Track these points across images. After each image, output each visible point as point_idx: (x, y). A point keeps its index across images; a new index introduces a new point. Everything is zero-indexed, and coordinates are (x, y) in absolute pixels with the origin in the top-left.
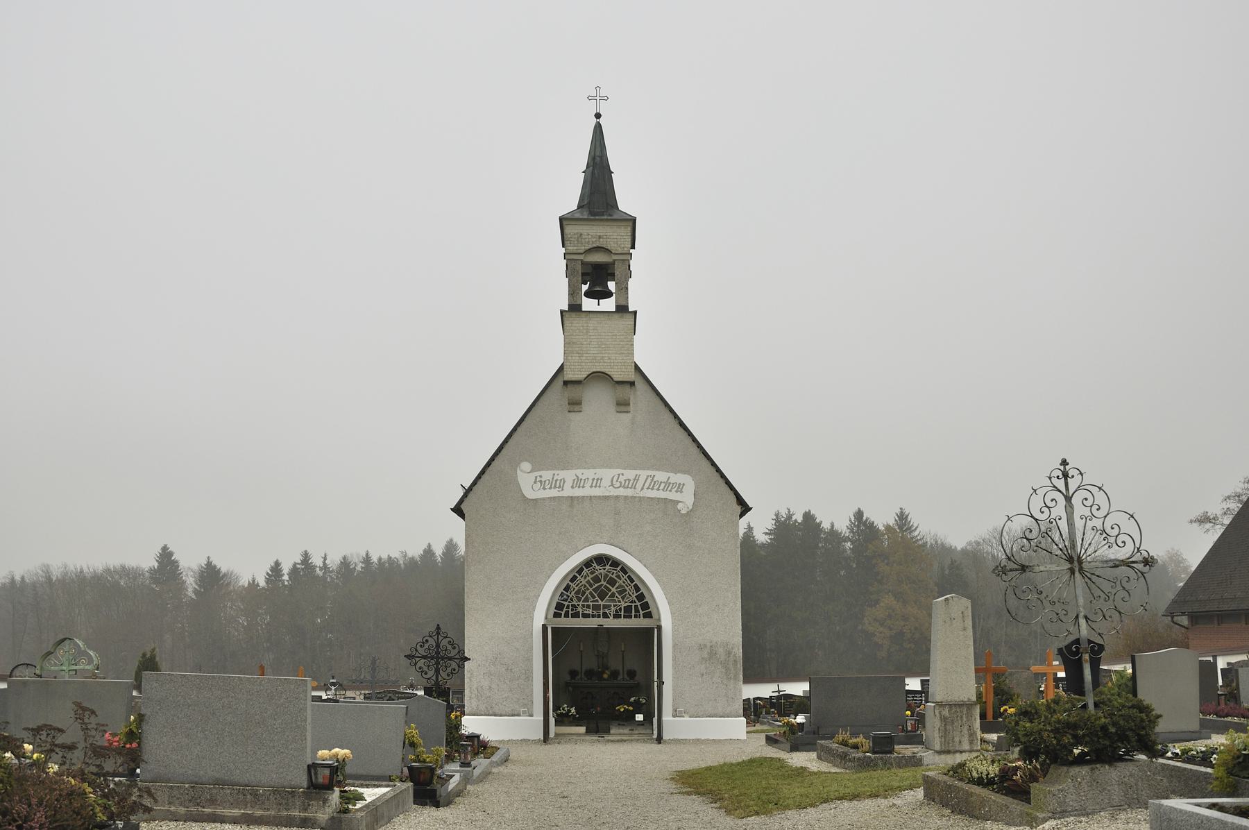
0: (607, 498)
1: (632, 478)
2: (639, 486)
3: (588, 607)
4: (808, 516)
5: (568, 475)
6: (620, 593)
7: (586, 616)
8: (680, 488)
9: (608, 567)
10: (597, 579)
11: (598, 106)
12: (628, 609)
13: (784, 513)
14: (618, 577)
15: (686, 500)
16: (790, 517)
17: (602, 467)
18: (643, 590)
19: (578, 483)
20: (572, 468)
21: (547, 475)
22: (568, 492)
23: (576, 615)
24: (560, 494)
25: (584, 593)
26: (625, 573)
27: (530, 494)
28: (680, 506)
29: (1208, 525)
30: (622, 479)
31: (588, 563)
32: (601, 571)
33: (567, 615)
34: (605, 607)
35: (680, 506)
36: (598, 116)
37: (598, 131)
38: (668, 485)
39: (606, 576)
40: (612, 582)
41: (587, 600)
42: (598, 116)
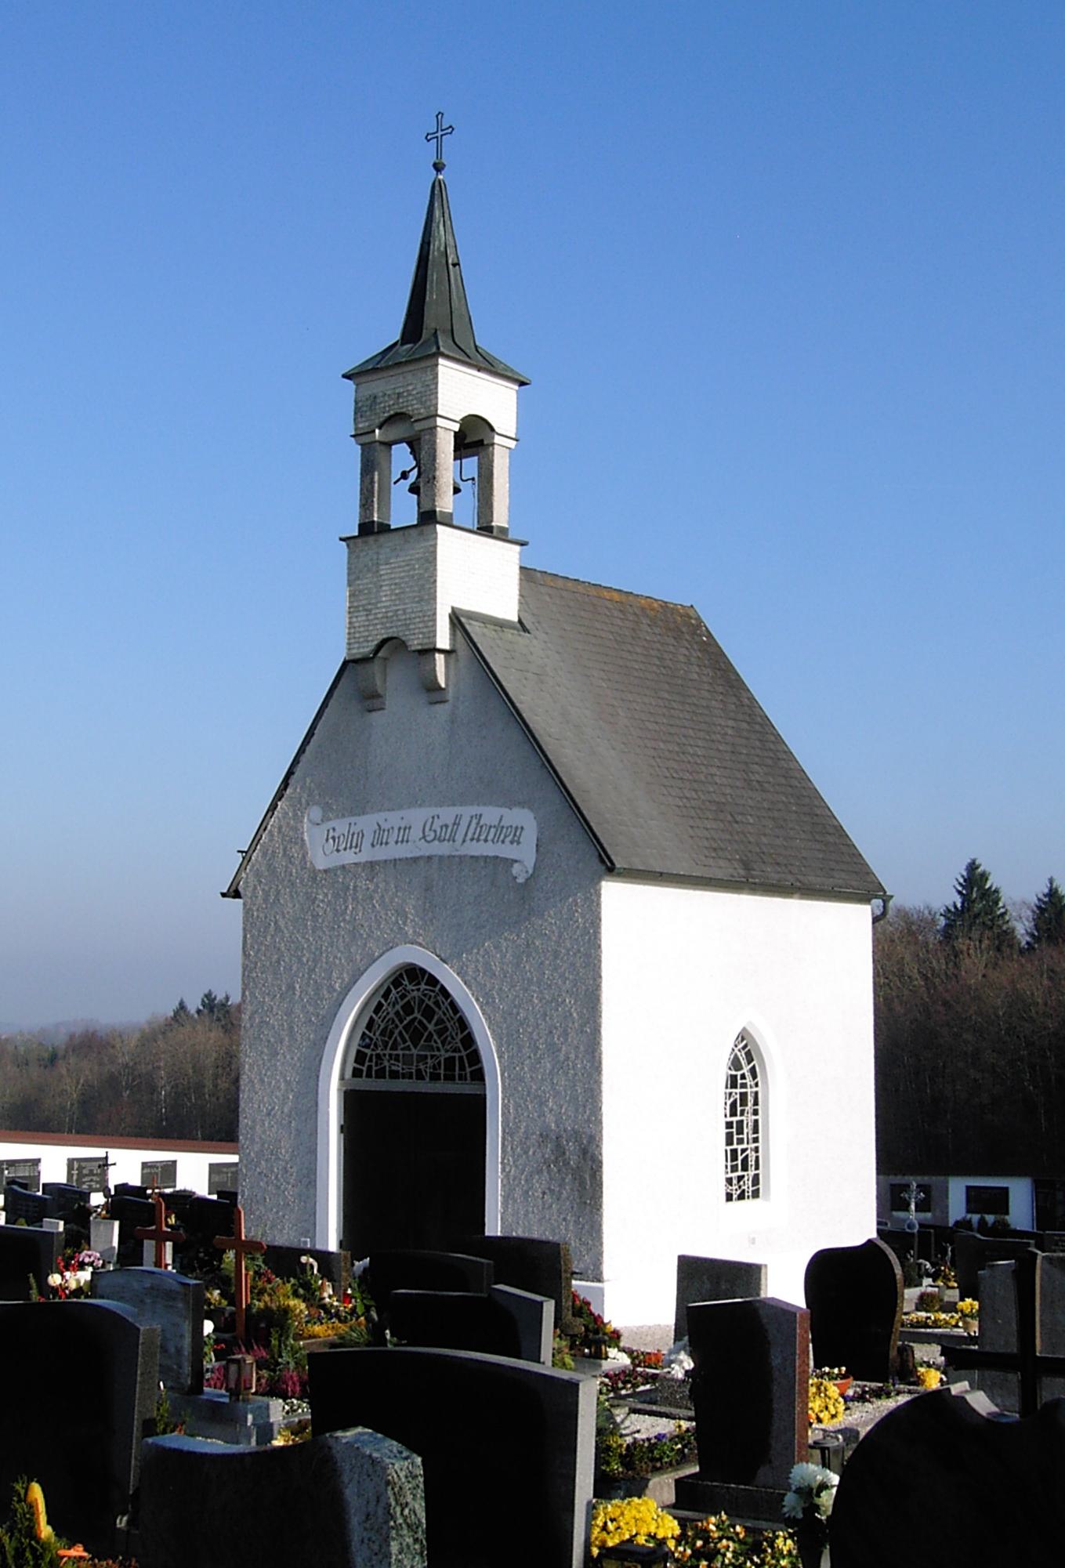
0: (415, 860)
1: (450, 822)
2: (459, 837)
5: (366, 823)
6: (440, 1033)
7: (394, 1075)
8: (516, 835)
9: (423, 986)
10: (408, 1009)
12: (450, 1062)
14: (437, 1003)
15: (524, 855)
19: (379, 841)
21: (341, 826)
23: (381, 1074)
25: (392, 1033)
32: (415, 992)
33: (369, 1075)
35: (516, 869)
37: (437, 192)
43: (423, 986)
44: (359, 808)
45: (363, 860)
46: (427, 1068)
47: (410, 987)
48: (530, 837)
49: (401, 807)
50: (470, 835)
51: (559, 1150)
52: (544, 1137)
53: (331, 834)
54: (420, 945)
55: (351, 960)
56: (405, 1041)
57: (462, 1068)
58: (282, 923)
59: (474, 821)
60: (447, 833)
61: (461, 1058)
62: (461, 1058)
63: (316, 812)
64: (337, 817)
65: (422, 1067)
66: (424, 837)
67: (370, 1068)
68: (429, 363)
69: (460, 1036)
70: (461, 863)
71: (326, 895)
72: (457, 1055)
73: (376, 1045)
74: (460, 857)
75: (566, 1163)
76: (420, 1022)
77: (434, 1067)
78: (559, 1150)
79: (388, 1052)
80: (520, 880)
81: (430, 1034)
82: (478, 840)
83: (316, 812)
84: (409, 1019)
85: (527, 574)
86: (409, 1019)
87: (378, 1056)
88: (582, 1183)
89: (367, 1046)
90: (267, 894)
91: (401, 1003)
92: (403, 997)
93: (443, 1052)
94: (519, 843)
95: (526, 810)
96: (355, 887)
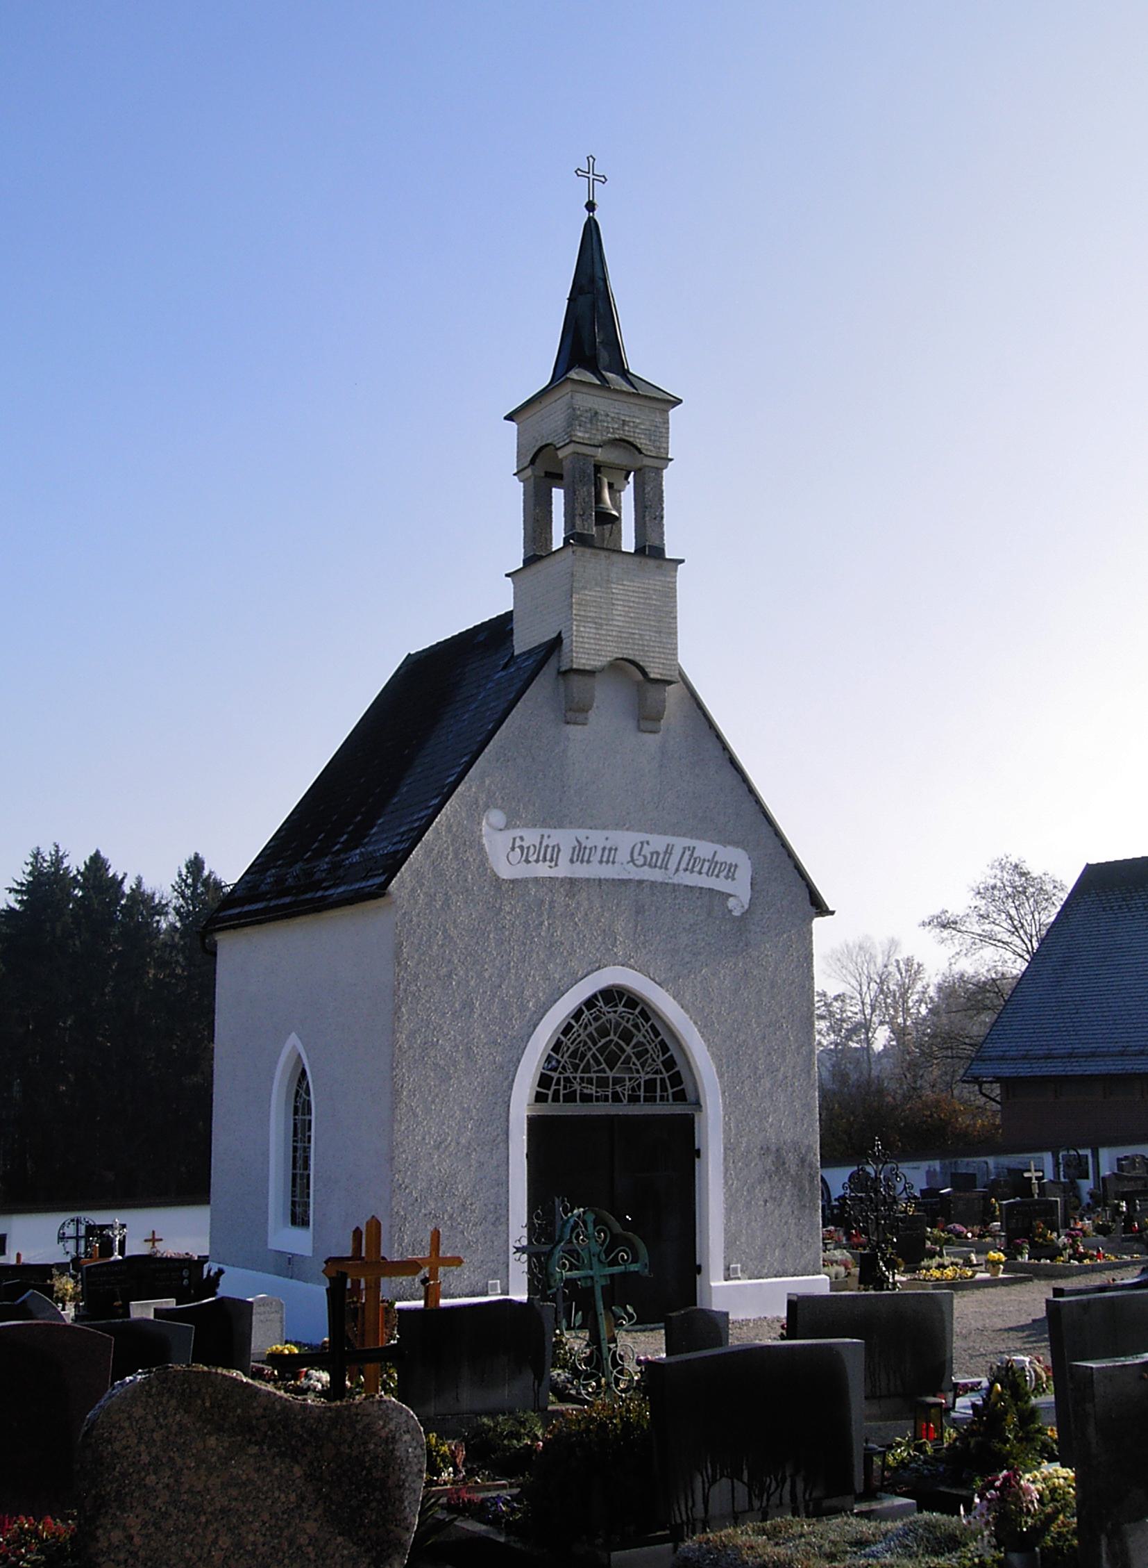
0: (624, 882)
1: (661, 850)
2: (672, 865)
3: (590, 1081)
4: (97, 863)
5: (564, 838)
6: (639, 1055)
7: (586, 1098)
8: (731, 871)
9: (620, 1009)
10: (603, 1032)
11: (591, 190)
12: (650, 1085)
13: (47, 852)
14: (636, 1026)
15: (740, 891)
16: (58, 860)
17: (619, 825)
18: (673, 1051)
19: (580, 854)
20: (573, 824)
21: (531, 837)
22: (563, 870)
23: (570, 1098)
24: (552, 873)
25: (583, 1056)
26: (647, 1019)
27: (505, 871)
28: (731, 903)
29: (946, 933)
30: (647, 850)
31: (590, 1003)
32: (610, 1014)
33: (556, 1099)
34: (617, 1081)
35: (731, 903)
36: (590, 206)
37: (591, 233)
38: (714, 866)
39: (618, 1024)
40: (627, 1036)
41: (587, 1069)
42: (590, 206)
43: (620, 1009)
44: (552, 818)
45: (561, 876)
46: (625, 1090)
47: (605, 1009)
48: (744, 874)
49: (605, 828)
50: (683, 865)
51: (780, 1161)
52: (765, 1150)
53: (518, 843)
54: (633, 968)
55: (547, 978)
56: (598, 1063)
57: (664, 1089)
58: (453, 932)
59: (688, 853)
60: (657, 860)
61: (662, 1080)
62: (662, 1080)
63: (497, 816)
64: (526, 826)
65: (619, 1090)
66: (632, 860)
67: (557, 1092)
68: (663, 406)
69: (662, 1058)
70: (674, 891)
71: (514, 907)
72: (658, 1076)
73: (564, 1067)
74: (674, 885)
75: (787, 1172)
76: (617, 1044)
77: (633, 1089)
78: (780, 1161)
79: (579, 1075)
80: (736, 913)
81: (629, 1057)
82: (692, 871)
83: (497, 816)
84: (603, 1041)
85: (509, 615)
86: (603, 1041)
87: (567, 1080)
88: (801, 1189)
89: (554, 1069)
90: (432, 898)
91: (595, 1025)
92: (596, 1019)
93: (642, 1074)
94: (733, 879)
95: (740, 850)
96: (552, 902)
